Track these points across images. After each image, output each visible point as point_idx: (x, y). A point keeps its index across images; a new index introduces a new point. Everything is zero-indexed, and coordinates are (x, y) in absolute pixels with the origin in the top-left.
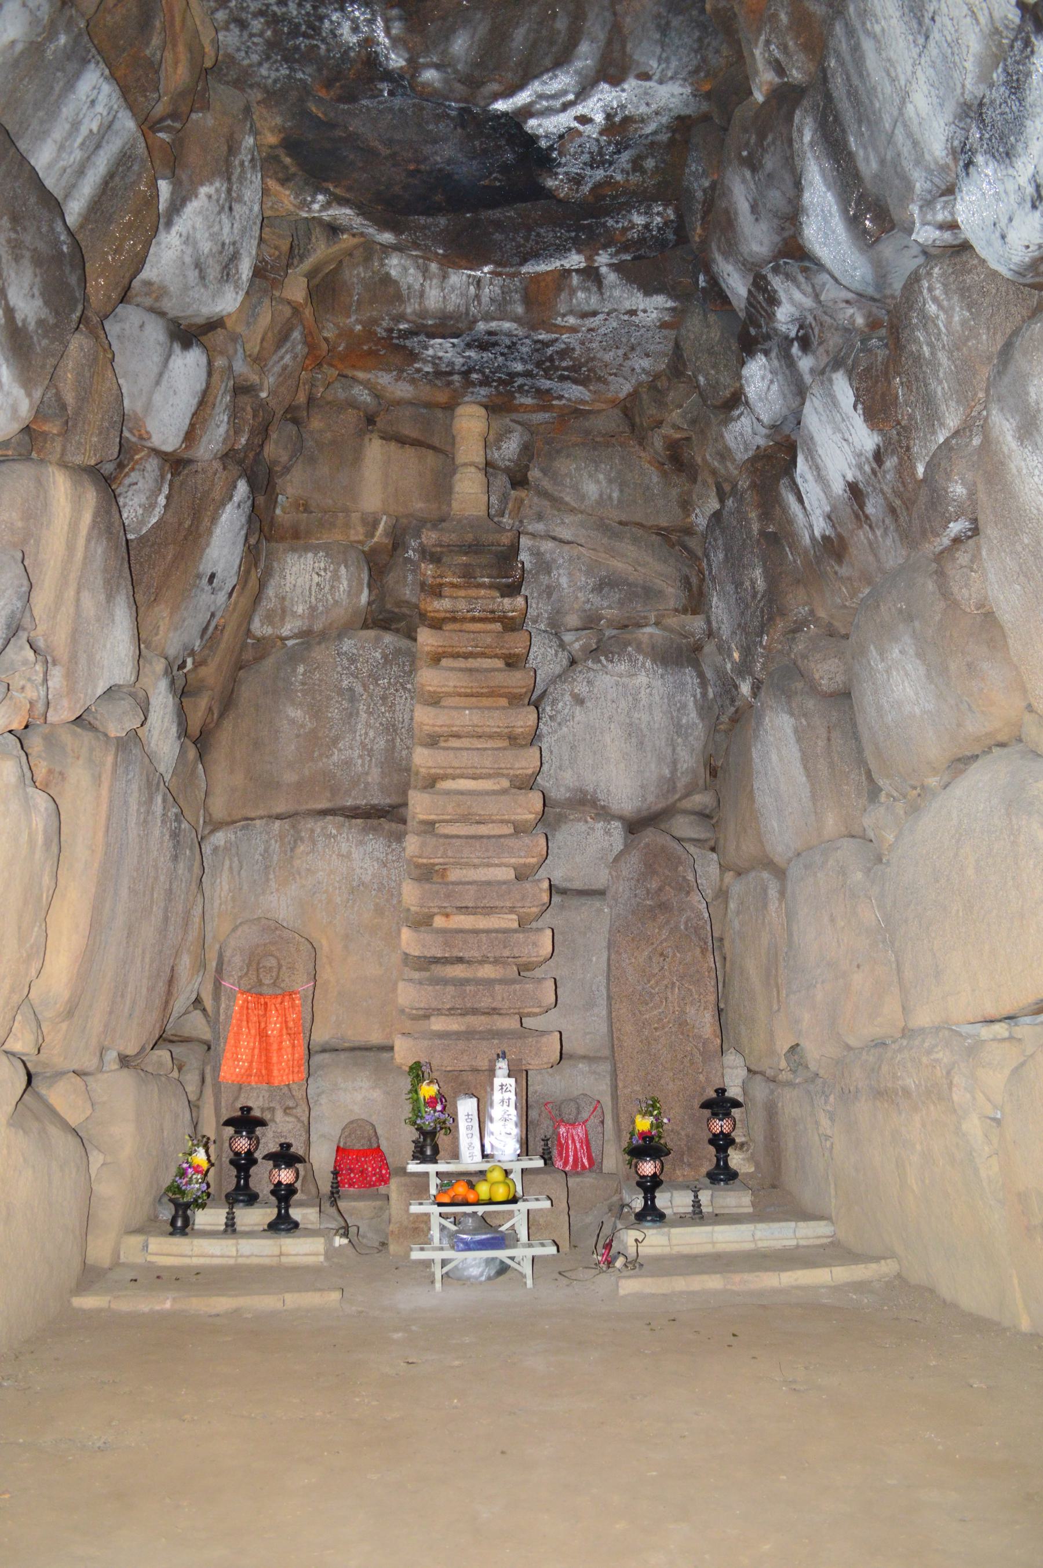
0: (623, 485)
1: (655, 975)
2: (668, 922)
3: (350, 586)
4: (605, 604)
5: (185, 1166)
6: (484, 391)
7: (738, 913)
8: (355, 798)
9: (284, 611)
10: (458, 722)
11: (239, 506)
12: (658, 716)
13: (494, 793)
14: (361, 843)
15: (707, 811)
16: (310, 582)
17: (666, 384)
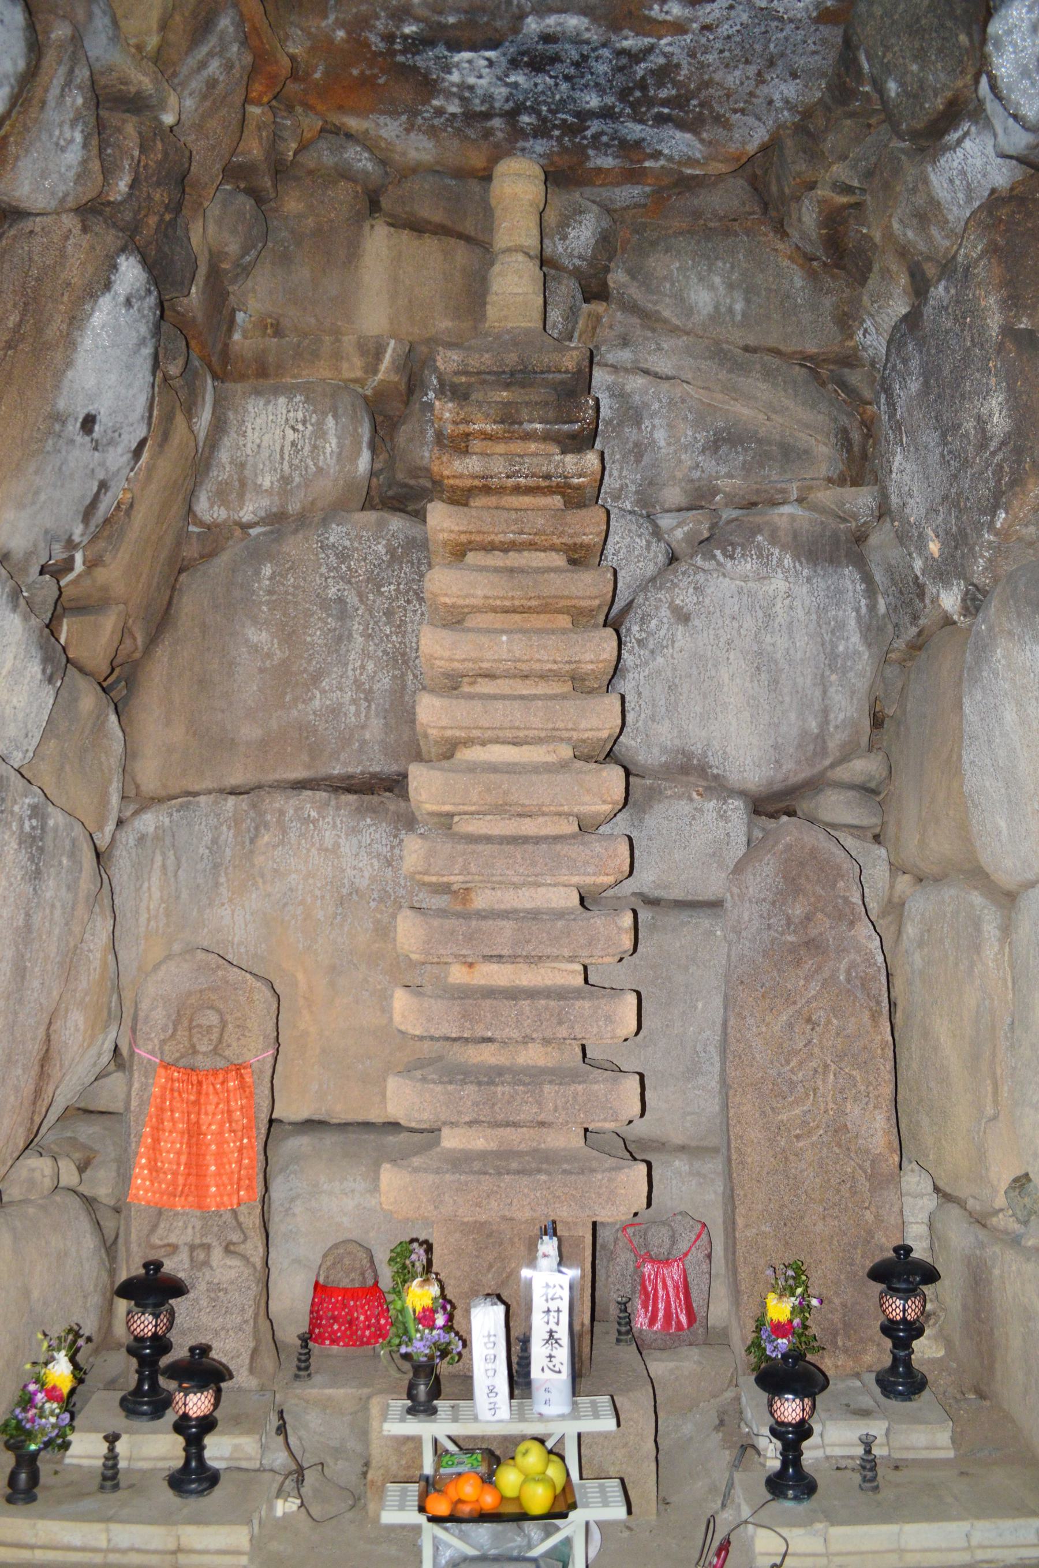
0: (750, 292)
1: (797, 1052)
2: (819, 969)
3: (341, 446)
4: (723, 470)
5: (32, 1387)
6: (540, 146)
7: (921, 944)
8: (345, 764)
9: (243, 484)
10: (489, 655)
11: (128, 303)
12: (802, 640)
13: (548, 768)
14: (355, 831)
15: (873, 785)
16: (281, 441)
17: (821, 122)
